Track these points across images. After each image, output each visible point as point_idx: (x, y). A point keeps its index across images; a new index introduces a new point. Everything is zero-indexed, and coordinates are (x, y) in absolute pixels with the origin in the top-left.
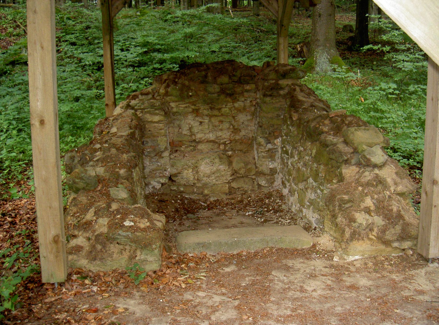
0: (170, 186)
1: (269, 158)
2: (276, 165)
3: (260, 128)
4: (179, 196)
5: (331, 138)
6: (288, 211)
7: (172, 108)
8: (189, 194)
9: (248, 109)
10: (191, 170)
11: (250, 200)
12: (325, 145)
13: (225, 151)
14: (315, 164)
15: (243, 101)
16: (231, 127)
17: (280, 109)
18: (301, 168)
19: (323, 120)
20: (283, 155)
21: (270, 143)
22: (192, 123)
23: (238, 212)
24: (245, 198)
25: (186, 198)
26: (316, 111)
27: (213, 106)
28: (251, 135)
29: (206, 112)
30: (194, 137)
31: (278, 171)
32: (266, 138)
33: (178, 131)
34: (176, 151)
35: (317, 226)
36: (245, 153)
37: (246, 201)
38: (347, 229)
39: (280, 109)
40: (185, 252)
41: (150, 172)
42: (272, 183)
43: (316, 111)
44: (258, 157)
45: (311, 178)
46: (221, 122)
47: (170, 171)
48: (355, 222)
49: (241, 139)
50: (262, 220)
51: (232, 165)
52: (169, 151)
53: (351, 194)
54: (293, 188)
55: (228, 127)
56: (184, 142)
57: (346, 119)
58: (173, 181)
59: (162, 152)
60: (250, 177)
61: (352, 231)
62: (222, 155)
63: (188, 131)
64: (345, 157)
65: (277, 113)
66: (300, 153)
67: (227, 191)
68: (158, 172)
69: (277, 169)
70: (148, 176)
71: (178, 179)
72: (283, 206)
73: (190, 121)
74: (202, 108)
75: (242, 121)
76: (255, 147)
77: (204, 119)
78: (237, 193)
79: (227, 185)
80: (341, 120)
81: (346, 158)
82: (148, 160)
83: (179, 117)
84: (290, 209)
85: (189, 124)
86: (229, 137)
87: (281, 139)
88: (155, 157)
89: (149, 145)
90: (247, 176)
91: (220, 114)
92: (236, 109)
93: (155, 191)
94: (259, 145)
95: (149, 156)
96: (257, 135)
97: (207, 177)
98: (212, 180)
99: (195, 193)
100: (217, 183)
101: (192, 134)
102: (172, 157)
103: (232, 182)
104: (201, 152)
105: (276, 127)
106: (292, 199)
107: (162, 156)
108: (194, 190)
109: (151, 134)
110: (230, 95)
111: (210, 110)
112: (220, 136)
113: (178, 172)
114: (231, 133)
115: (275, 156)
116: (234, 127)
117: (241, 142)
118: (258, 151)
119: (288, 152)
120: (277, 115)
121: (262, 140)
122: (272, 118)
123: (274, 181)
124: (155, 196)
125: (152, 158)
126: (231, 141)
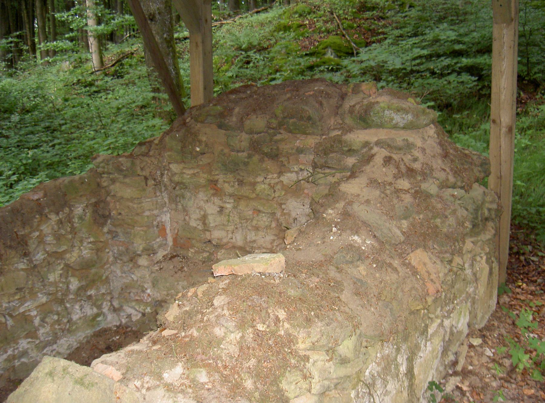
30: (208, 236)
63: (198, 222)
74: (221, 178)
77: (225, 202)
82: (118, 266)
85: (200, 208)
91: (254, 195)
101: (206, 229)
110: (274, 156)
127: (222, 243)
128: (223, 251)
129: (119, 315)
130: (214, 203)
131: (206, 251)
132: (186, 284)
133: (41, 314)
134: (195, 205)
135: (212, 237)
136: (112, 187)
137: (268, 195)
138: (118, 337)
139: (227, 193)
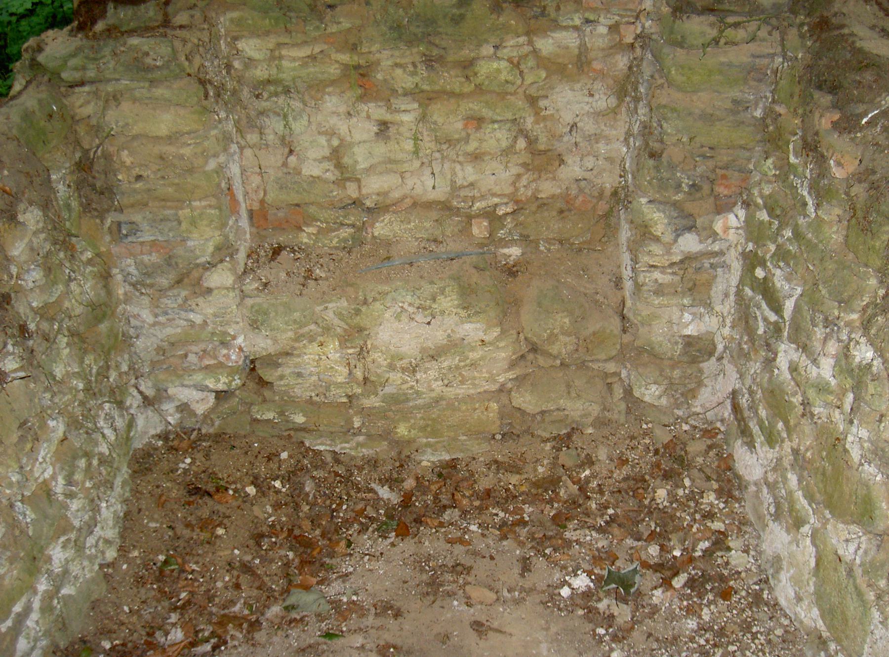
1: (684, 295)
3: (651, 162)
7: (250, 63)
9: (597, 65)
11: (588, 480)
15: (576, 28)
16: (521, 144)
17: (753, 73)
21: (690, 229)
22: (343, 127)
24: (569, 463)
27: (435, 52)
28: (609, 181)
29: (404, 80)
30: (352, 191)
31: (720, 347)
32: (675, 204)
33: (285, 164)
34: (277, 251)
39: (753, 73)
41: (161, 350)
42: (692, 394)
44: (638, 287)
46: (479, 121)
47: (248, 342)
49: (567, 198)
51: (518, 313)
52: (241, 256)
55: (504, 144)
56: (312, 210)
58: (263, 383)
62: (475, 277)
63: (326, 165)
65: (735, 93)
67: (495, 428)
68: (195, 348)
70: (153, 364)
71: (281, 377)
73: (334, 120)
75: (568, 117)
76: (625, 234)
77: (398, 111)
79: (494, 406)
83: (281, 100)
85: (331, 133)
86: (509, 190)
88: (175, 291)
89: (147, 237)
90: (582, 365)
92: (542, 62)
93: (189, 424)
94: (644, 233)
97: (404, 370)
98: (430, 381)
100: (450, 392)
101: (346, 174)
102: (251, 285)
104: (383, 255)
105: (724, 157)
108: (349, 421)
111: (422, 70)
112: (472, 185)
113: (278, 348)
114: (521, 170)
115: (709, 284)
116: (531, 142)
117: (565, 207)
118: (635, 260)
120: (735, 102)
121: (659, 221)
122: (708, 118)
123: (700, 384)
127: (388, 202)
128: (387, 217)
129: (159, 412)
130: (368, 117)
131: (348, 225)
132: (346, 304)
133: (63, 469)
134: (314, 127)
135: (364, 191)
136: (111, 115)
137: (507, 82)
138: (188, 461)
139: (400, 91)
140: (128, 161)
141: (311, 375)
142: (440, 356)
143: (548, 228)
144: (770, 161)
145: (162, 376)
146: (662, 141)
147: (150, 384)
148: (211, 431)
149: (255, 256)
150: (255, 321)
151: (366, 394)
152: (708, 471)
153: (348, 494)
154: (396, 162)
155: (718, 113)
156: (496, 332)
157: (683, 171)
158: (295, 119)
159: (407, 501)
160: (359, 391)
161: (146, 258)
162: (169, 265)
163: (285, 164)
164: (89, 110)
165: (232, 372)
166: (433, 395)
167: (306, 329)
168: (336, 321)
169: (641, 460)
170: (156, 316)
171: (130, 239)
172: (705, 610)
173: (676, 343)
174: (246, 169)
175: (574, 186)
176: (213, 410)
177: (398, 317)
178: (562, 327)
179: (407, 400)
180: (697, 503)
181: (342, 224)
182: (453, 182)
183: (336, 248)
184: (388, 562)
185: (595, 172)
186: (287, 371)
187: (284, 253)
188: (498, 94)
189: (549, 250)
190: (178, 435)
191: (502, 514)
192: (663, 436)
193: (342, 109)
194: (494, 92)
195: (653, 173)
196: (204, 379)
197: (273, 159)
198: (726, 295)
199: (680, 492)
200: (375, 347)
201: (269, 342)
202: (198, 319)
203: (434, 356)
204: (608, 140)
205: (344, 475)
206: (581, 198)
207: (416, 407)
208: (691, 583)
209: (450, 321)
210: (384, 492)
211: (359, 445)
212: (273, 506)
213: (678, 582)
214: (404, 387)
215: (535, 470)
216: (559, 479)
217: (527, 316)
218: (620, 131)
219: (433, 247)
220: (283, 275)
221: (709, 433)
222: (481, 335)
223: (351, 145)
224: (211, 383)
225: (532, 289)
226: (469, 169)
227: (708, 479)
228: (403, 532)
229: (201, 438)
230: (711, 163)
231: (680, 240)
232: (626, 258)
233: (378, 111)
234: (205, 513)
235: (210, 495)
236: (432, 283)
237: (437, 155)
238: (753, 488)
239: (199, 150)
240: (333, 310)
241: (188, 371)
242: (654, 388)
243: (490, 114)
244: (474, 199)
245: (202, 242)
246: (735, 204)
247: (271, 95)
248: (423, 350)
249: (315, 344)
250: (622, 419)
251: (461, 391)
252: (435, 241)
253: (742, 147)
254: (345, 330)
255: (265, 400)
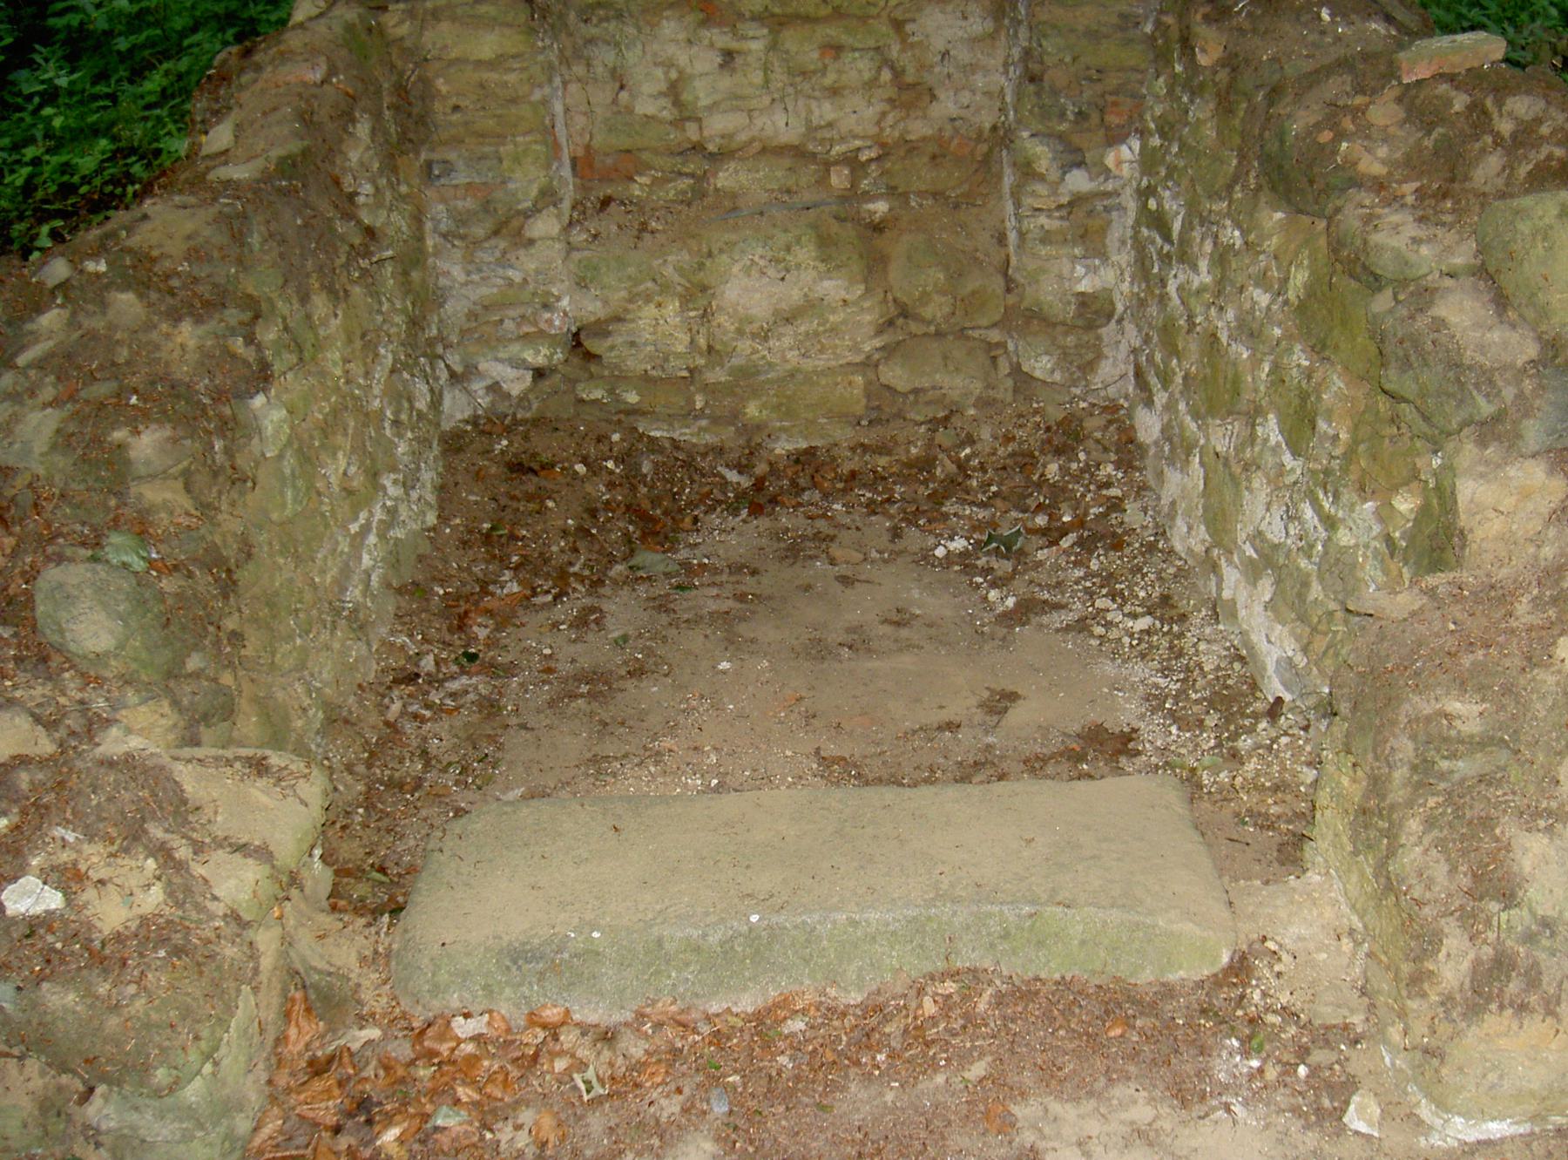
0: (574, 382)
1: (1074, 245)
2: (1108, 276)
3: (1032, 88)
4: (616, 437)
5: (1398, 237)
6: (1151, 548)
8: (670, 419)
10: (673, 306)
11: (968, 458)
12: (1354, 267)
13: (852, 195)
14: (1298, 347)
16: (886, 75)
18: (1224, 340)
19: (1359, 100)
20: (1145, 232)
21: (1080, 164)
22: (683, 59)
23: (896, 533)
24: (947, 443)
25: (652, 440)
26: (1325, 15)
28: (986, 120)
30: (692, 133)
31: (1120, 308)
32: (1060, 137)
33: (615, 102)
34: (606, 202)
35: (1287, 697)
36: (956, 206)
37: (947, 462)
38: (1454, 939)
40: (436, 1004)
41: (472, 315)
42: (1089, 367)
43: (1325, 15)
44: (1022, 235)
45: (1272, 419)
46: (836, 49)
47: (572, 306)
48: (1509, 898)
49: (938, 139)
50: (1010, 602)
51: (885, 271)
52: (566, 205)
53: (1507, 690)
54: (1181, 426)
55: (867, 76)
56: (645, 156)
57: (1500, 104)
58: (590, 357)
59: (527, 215)
60: (976, 334)
61: (1488, 951)
62: (835, 227)
63: (663, 102)
64: (1481, 401)
66: (1222, 257)
67: (859, 409)
68: (512, 313)
69: (1117, 297)
71: (612, 348)
72: (1133, 515)
73: (671, 50)
75: (939, 44)
76: (1008, 179)
77: (744, 38)
78: (912, 415)
79: (859, 379)
80: (1471, 108)
81: (1486, 408)
82: (458, 254)
83: (612, 26)
84: (1161, 533)
85: (669, 64)
86: (873, 130)
87: (1136, 145)
88: (493, 242)
89: (461, 178)
90: (961, 333)
93: (503, 407)
94: (1027, 171)
95: (463, 238)
96: (1019, 121)
97: (754, 336)
98: (784, 351)
99: (696, 418)
100: (808, 365)
101: (685, 114)
102: (578, 236)
103: (887, 359)
104: (730, 207)
105: (1113, 81)
106: (1173, 477)
107: (528, 234)
108: (690, 401)
109: (466, 123)
112: (830, 125)
114: (887, 107)
115: (1103, 231)
116: (898, 74)
118: (1018, 205)
119: (1170, 230)
120: (1122, 16)
121: (1042, 155)
122: (1093, 35)
123: (1100, 356)
124: (500, 436)
125: (477, 243)
126: (885, 152)
127: (734, 146)
128: (732, 165)
130: (712, 45)
131: (687, 175)
132: (687, 257)
135: (706, 133)
136: (428, 37)
138: (505, 442)
139: (747, 15)
140: (444, 89)
141: (645, 344)
142: (794, 318)
143: (919, 178)
144: (1161, 80)
145: (471, 349)
146: (1042, 63)
147: (457, 357)
148: (528, 415)
149: (580, 208)
150: (584, 279)
151: (710, 366)
152: (1106, 443)
153: (690, 478)
154: (742, 98)
155: (1104, 30)
156: (859, 290)
157: (1067, 97)
158: (628, 48)
159: (759, 485)
160: (702, 362)
161: (460, 204)
162: (486, 211)
163: (615, 102)
164: (404, 30)
165: (553, 340)
166: (788, 367)
167: (642, 287)
168: (677, 278)
169: (1029, 437)
170: (468, 273)
171: (443, 181)
172: (1094, 561)
173: (1069, 303)
174: (574, 110)
175: (948, 127)
176: (530, 390)
177: (747, 271)
178: (935, 285)
179: (758, 373)
180: (1092, 475)
181: (680, 174)
182: (808, 121)
183: (673, 201)
184: (740, 535)
185: (972, 109)
186: (619, 340)
187: (613, 207)
188: (859, 18)
189: (921, 205)
190: (490, 420)
191: (869, 495)
192: (1055, 414)
193: (682, 36)
194: (855, 16)
195: (1034, 100)
196: (522, 351)
197: (602, 96)
198: (1123, 243)
199: (1074, 466)
200: (720, 308)
201: (599, 304)
202: (516, 276)
203: (789, 318)
204: (987, 71)
205: (686, 461)
206: (956, 141)
207: (768, 381)
208: (1080, 542)
209: (808, 276)
210: (732, 476)
211: (701, 429)
212: (607, 486)
213: (1066, 543)
214: (754, 357)
215: (908, 451)
216: (936, 458)
217: (895, 273)
218: (996, 61)
219: (786, 198)
220: (614, 228)
221: (1112, 408)
222: (843, 294)
223: (691, 77)
224: (529, 356)
225: (899, 247)
226: (827, 106)
227: (1106, 450)
228: (756, 510)
229: (516, 422)
230: (1099, 88)
231: (1068, 176)
232: (1009, 207)
233: (723, 39)
234: (531, 488)
235: (535, 473)
236: (786, 231)
237: (790, 90)
238: (1152, 451)
239: (524, 76)
240: (673, 263)
241: (503, 341)
242: (1045, 359)
243: (851, 40)
244: (832, 142)
245: (525, 183)
246: (1128, 135)
247: (601, 20)
248: (776, 313)
249: (652, 306)
250: (1009, 398)
251: (821, 362)
252: (789, 191)
253: (1135, 69)
254: (687, 289)
255: (592, 376)
